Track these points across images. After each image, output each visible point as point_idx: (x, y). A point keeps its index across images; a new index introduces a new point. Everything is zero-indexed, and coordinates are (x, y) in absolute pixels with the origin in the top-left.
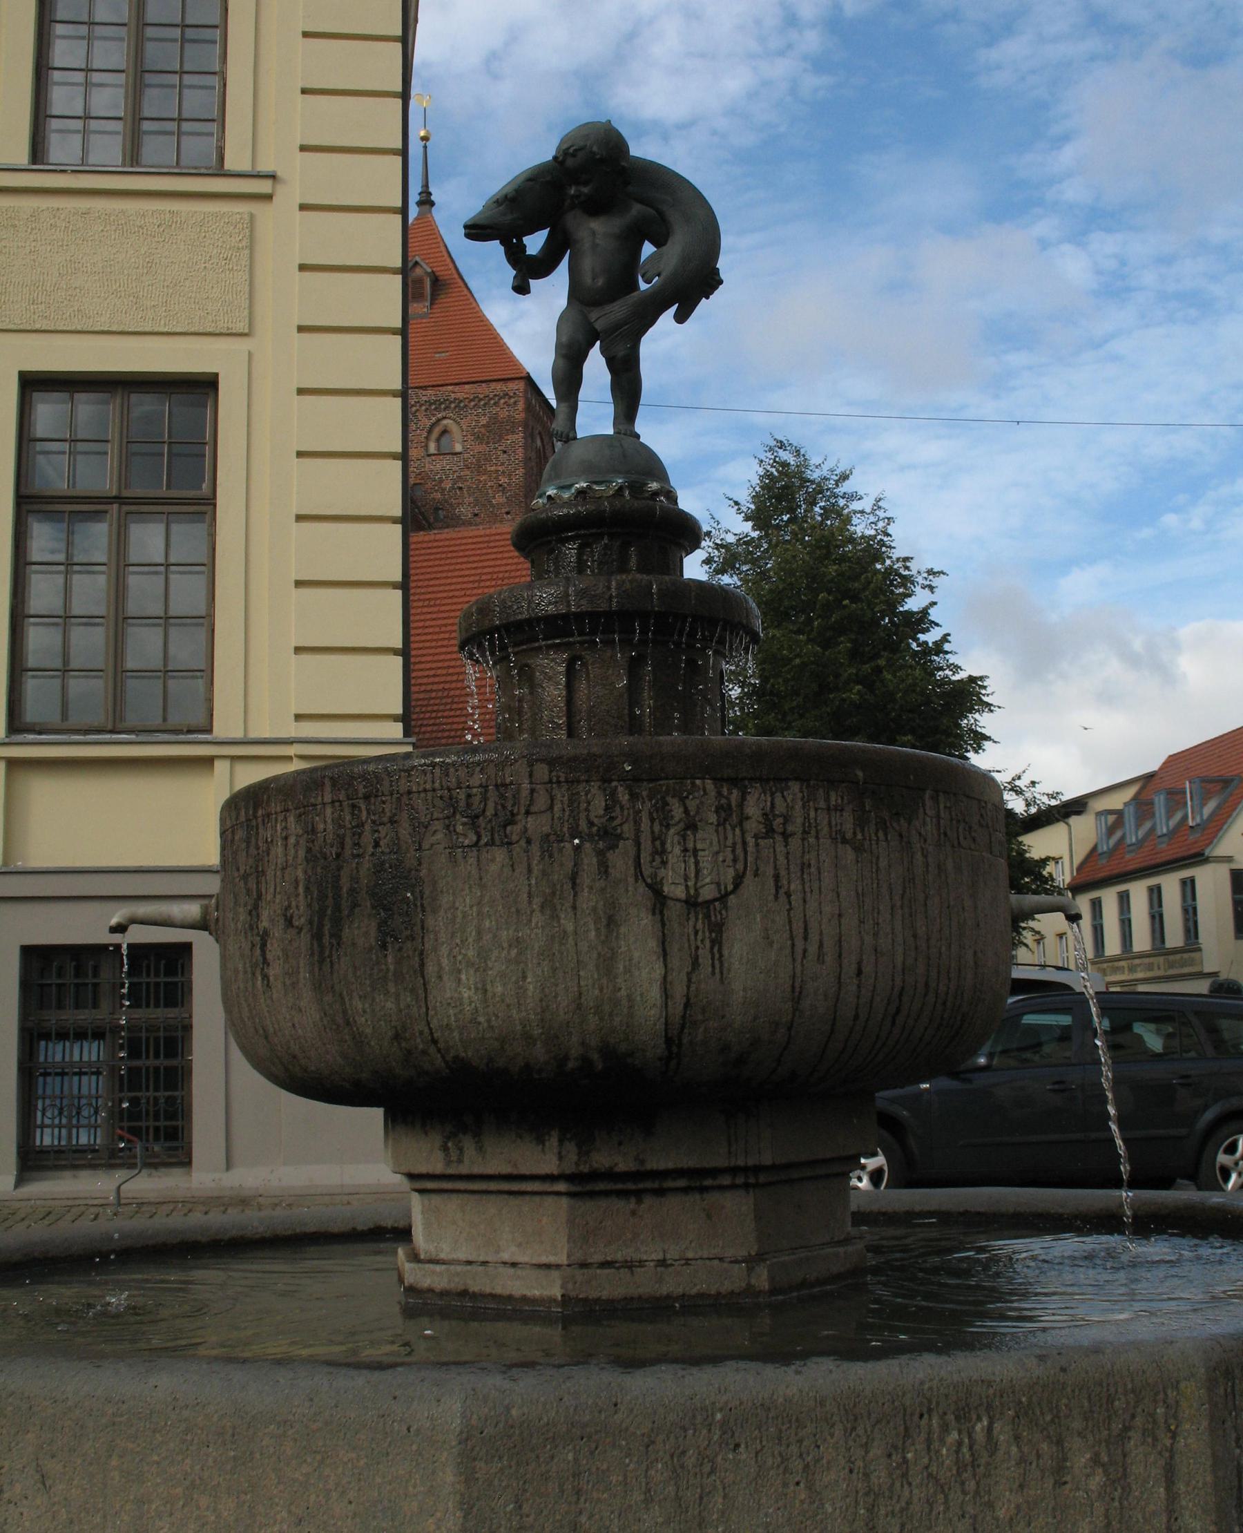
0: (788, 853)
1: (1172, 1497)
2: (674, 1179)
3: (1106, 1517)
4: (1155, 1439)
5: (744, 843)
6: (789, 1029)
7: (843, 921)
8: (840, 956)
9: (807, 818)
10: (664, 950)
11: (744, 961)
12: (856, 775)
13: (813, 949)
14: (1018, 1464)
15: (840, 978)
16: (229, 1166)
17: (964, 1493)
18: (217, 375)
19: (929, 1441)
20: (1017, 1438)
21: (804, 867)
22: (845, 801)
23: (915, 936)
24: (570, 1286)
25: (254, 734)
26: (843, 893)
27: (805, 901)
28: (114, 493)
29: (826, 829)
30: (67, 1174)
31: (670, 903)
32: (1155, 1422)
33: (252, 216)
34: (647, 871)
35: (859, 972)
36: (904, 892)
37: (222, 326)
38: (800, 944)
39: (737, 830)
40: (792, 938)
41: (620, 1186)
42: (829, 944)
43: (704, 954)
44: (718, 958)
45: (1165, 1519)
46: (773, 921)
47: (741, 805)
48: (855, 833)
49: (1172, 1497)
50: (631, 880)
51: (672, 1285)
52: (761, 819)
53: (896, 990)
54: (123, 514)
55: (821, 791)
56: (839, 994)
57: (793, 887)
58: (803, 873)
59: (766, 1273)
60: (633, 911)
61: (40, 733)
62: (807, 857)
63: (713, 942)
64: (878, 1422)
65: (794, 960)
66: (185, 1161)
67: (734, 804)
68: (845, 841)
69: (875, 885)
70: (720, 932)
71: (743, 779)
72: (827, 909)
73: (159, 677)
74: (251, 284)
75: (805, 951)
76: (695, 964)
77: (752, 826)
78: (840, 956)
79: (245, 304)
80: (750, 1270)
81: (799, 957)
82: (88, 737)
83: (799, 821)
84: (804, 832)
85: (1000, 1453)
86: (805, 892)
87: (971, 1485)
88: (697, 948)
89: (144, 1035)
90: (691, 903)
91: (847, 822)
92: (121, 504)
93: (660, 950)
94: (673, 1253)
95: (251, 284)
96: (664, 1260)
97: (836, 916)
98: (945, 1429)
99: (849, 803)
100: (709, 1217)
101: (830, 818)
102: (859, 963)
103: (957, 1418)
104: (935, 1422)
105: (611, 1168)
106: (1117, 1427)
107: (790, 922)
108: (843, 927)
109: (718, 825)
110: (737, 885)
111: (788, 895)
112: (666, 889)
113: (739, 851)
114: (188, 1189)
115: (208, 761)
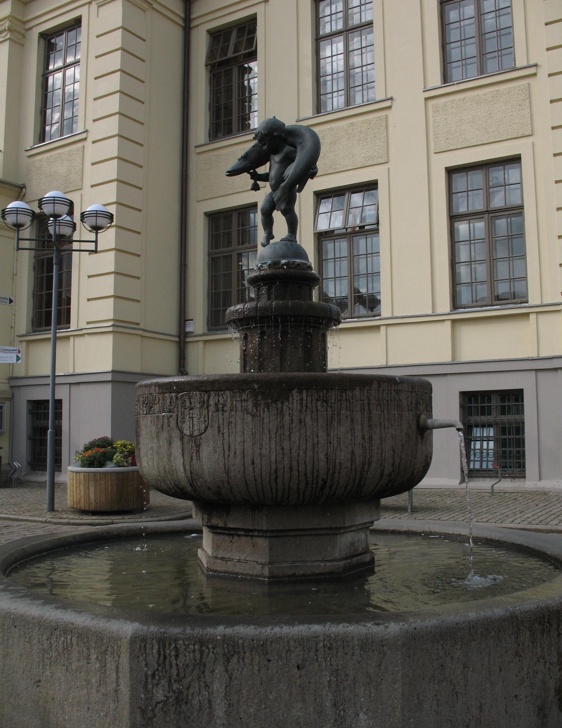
0: (223, 418)
1: (118, 678)
2: (240, 531)
3: (100, 678)
4: (114, 657)
5: (208, 414)
6: (228, 483)
7: (245, 444)
8: (244, 457)
9: (232, 404)
10: (183, 453)
11: (207, 458)
12: (254, 387)
13: (232, 454)
14: (78, 653)
15: (244, 465)
16: (540, 479)
17: (65, 658)
18: (520, 154)
19: (56, 638)
20: (78, 644)
21: (229, 423)
22: (249, 397)
23: (282, 449)
24: (209, 564)
25: (545, 302)
26: (246, 433)
27: (229, 436)
28: (485, 209)
29: (240, 408)
30: (481, 479)
31: (185, 436)
32: (114, 650)
33: (529, 84)
34: (180, 424)
35: (253, 463)
36: (277, 431)
37: (520, 134)
38: (227, 453)
39: (206, 410)
40: (224, 450)
41: (224, 532)
42: (238, 452)
43: (194, 455)
44: (198, 457)
45: (115, 685)
46: (217, 444)
47: (208, 401)
48: (253, 410)
49: (118, 678)
50: (175, 428)
51: (239, 569)
52: (214, 406)
53: (272, 470)
54: (489, 217)
55: (238, 394)
56: (245, 471)
57: (225, 431)
58: (229, 425)
59: (267, 569)
60: (175, 439)
61: (465, 308)
62: (231, 419)
63: (197, 451)
64: (45, 628)
65: (225, 458)
66: (522, 476)
67: (205, 400)
68: (248, 413)
69: (261, 429)
70: (199, 447)
71: (209, 391)
72: (238, 439)
73: (508, 282)
74: (531, 114)
75: (229, 455)
76: (192, 459)
77: (212, 408)
78: (244, 457)
79: (529, 122)
80: (263, 568)
81: (226, 457)
82: (483, 308)
83: (229, 405)
84: (231, 410)
85: (74, 648)
86: (229, 433)
87: (66, 656)
88: (192, 453)
89: (507, 426)
90: (191, 436)
91: (250, 405)
92: (489, 213)
93: (182, 453)
94: (242, 558)
95: (531, 114)
96: (240, 560)
97: (242, 442)
98: (61, 636)
99: (250, 398)
100: (254, 546)
101: (242, 404)
102: (253, 460)
103: (64, 633)
104: (58, 632)
105: (217, 525)
106: (104, 649)
107: (223, 444)
108: (245, 446)
109: (200, 408)
110: (205, 431)
111: (223, 434)
112: (184, 431)
113: (206, 418)
114: (523, 487)
115: (527, 315)
